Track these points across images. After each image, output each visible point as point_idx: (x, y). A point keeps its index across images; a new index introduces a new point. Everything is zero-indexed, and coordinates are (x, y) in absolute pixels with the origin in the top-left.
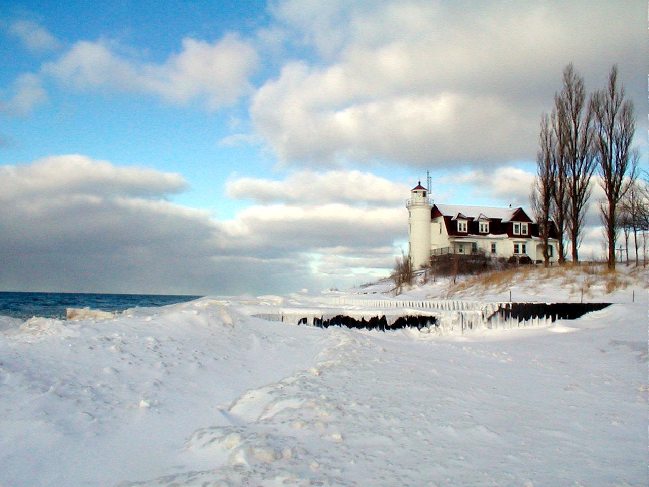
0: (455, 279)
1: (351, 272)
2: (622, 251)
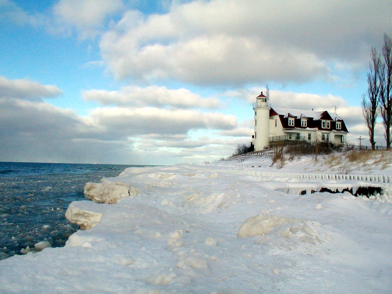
0: (316, 157)
1: (156, 150)
2: (361, 140)
